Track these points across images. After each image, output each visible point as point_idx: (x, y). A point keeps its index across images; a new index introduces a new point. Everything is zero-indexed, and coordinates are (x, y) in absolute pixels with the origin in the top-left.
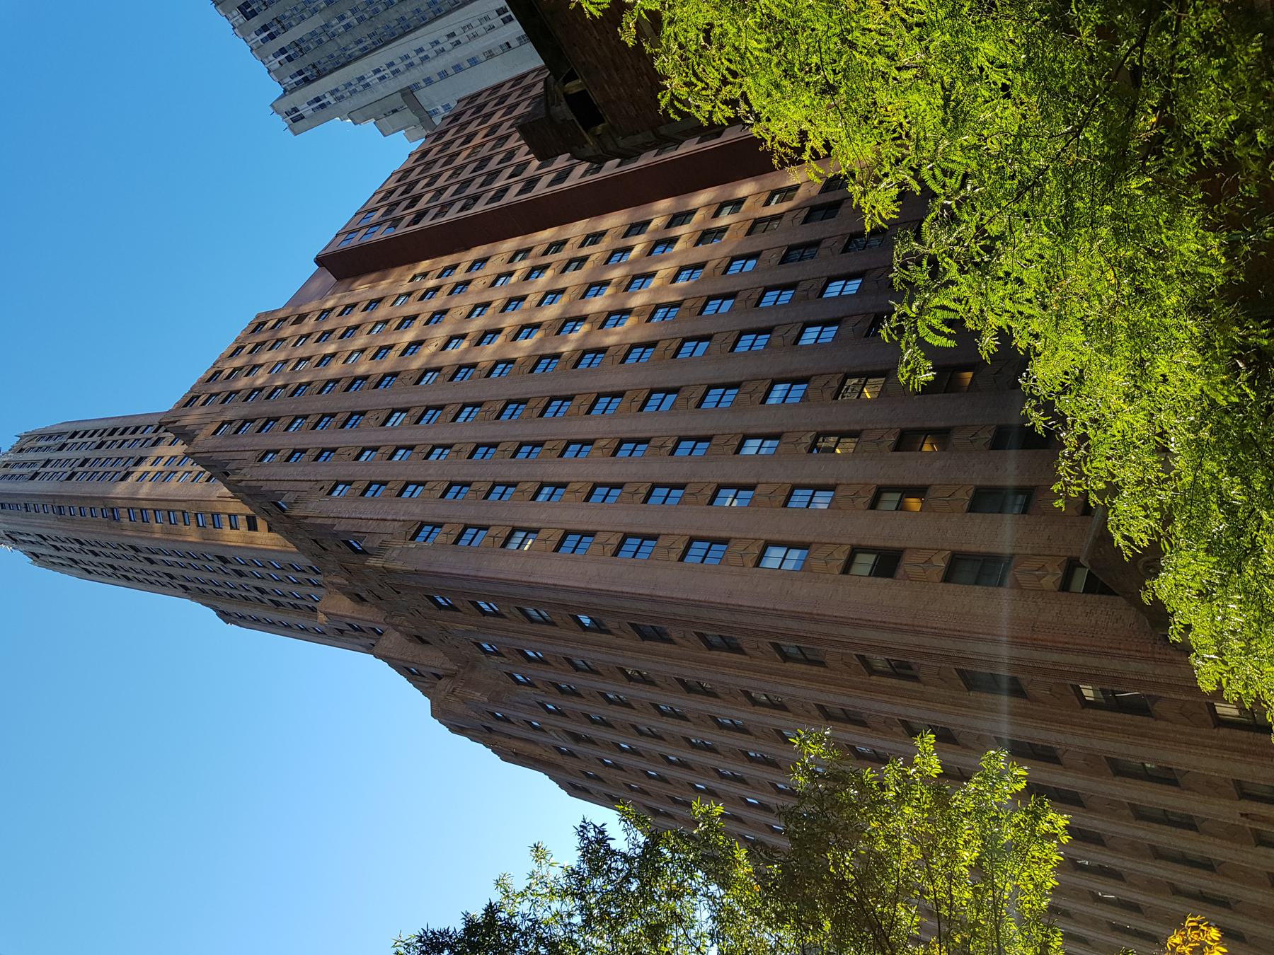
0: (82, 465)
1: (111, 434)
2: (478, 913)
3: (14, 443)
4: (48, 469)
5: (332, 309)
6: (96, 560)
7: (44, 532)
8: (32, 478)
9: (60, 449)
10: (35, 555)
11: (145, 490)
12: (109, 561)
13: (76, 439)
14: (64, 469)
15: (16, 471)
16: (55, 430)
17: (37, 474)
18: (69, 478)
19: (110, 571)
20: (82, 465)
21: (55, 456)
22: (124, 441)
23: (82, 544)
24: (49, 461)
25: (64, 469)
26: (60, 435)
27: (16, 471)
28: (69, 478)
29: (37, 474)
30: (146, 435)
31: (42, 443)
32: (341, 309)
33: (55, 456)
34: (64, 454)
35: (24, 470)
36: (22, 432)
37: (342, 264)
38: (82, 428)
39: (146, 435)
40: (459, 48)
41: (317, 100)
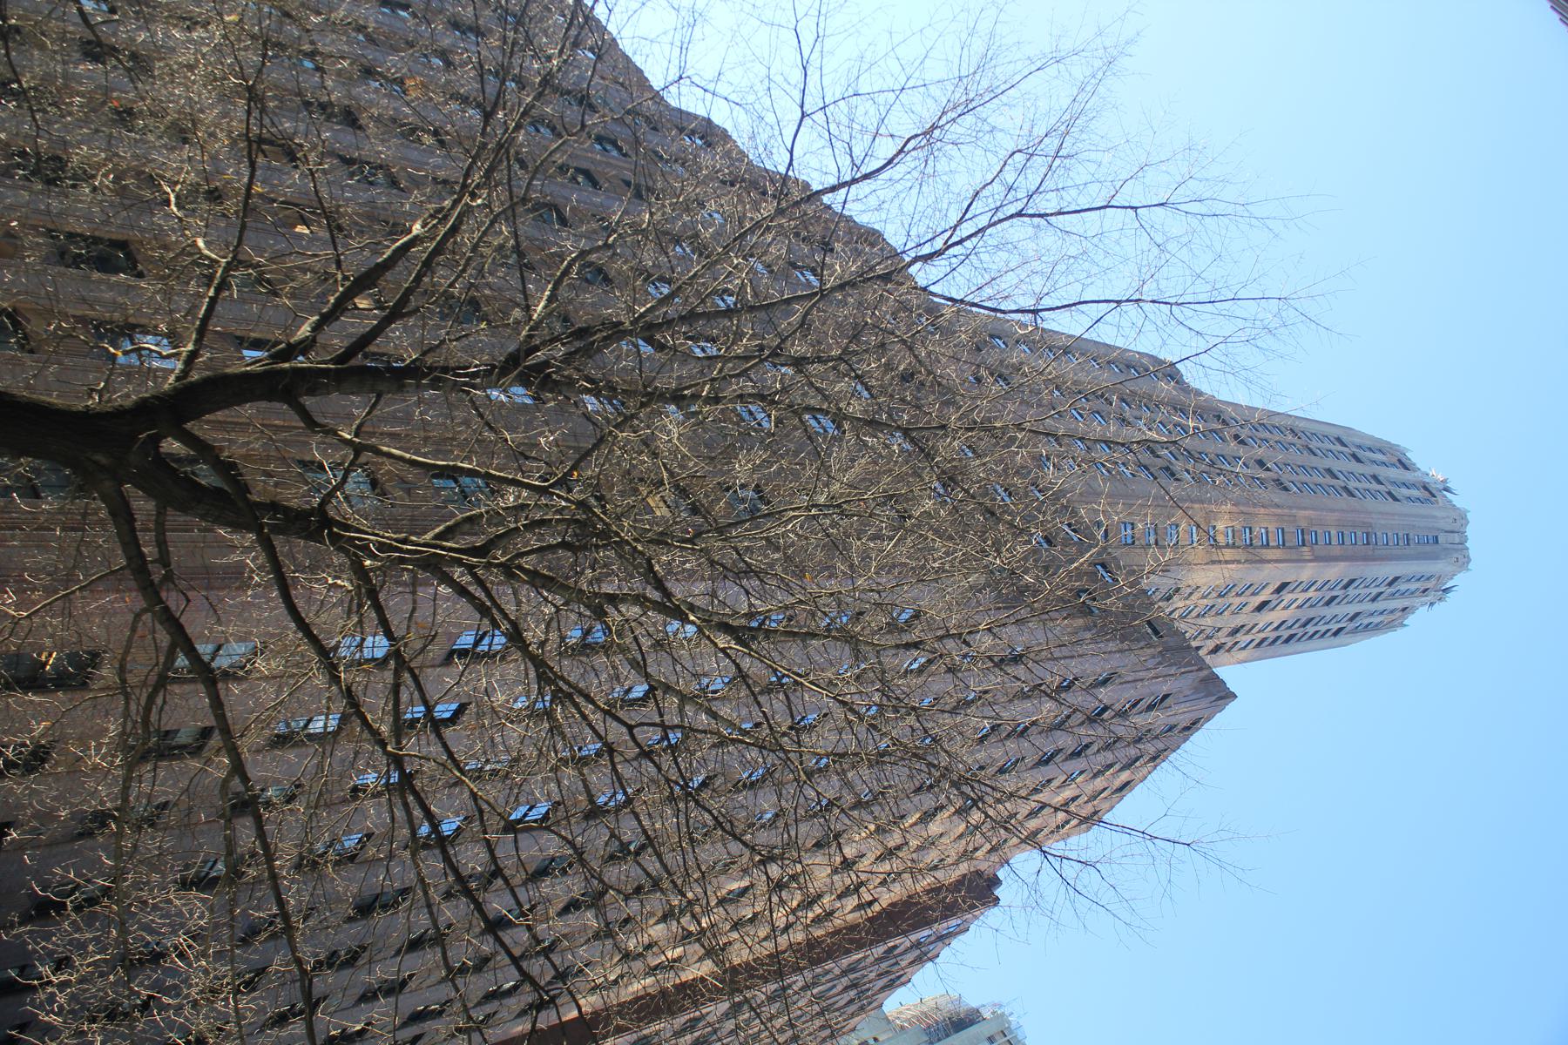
0: (1334, 598)
1: (1292, 636)
2: (998, 892)
3: (1411, 617)
4: (1375, 591)
5: (1122, 769)
6: (1329, 463)
7: (1391, 506)
8: (1396, 579)
9: (1357, 615)
10: (1404, 465)
11: (1307, 572)
12: (1314, 461)
13: (1335, 627)
14: (1357, 592)
15: (1413, 586)
16: (1359, 636)
17: (1390, 584)
18: (1352, 581)
19: (1314, 444)
20: (1334, 598)
21: (1368, 607)
22: (1277, 628)
23: (1346, 489)
24: (1373, 600)
25: (1357, 592)
26: (1355, 631)
27: (1413, 586)
28: (1352, 581)
29: (1390, 584)
30: (1249, 638)
31: (1376, 620)
32: (1089, 752)
33: (1368, 607)
34: (1352, 609)
35: (1403, 587)
36: (1400, 631)
38: (1329, 640)
39: (1249, 638)
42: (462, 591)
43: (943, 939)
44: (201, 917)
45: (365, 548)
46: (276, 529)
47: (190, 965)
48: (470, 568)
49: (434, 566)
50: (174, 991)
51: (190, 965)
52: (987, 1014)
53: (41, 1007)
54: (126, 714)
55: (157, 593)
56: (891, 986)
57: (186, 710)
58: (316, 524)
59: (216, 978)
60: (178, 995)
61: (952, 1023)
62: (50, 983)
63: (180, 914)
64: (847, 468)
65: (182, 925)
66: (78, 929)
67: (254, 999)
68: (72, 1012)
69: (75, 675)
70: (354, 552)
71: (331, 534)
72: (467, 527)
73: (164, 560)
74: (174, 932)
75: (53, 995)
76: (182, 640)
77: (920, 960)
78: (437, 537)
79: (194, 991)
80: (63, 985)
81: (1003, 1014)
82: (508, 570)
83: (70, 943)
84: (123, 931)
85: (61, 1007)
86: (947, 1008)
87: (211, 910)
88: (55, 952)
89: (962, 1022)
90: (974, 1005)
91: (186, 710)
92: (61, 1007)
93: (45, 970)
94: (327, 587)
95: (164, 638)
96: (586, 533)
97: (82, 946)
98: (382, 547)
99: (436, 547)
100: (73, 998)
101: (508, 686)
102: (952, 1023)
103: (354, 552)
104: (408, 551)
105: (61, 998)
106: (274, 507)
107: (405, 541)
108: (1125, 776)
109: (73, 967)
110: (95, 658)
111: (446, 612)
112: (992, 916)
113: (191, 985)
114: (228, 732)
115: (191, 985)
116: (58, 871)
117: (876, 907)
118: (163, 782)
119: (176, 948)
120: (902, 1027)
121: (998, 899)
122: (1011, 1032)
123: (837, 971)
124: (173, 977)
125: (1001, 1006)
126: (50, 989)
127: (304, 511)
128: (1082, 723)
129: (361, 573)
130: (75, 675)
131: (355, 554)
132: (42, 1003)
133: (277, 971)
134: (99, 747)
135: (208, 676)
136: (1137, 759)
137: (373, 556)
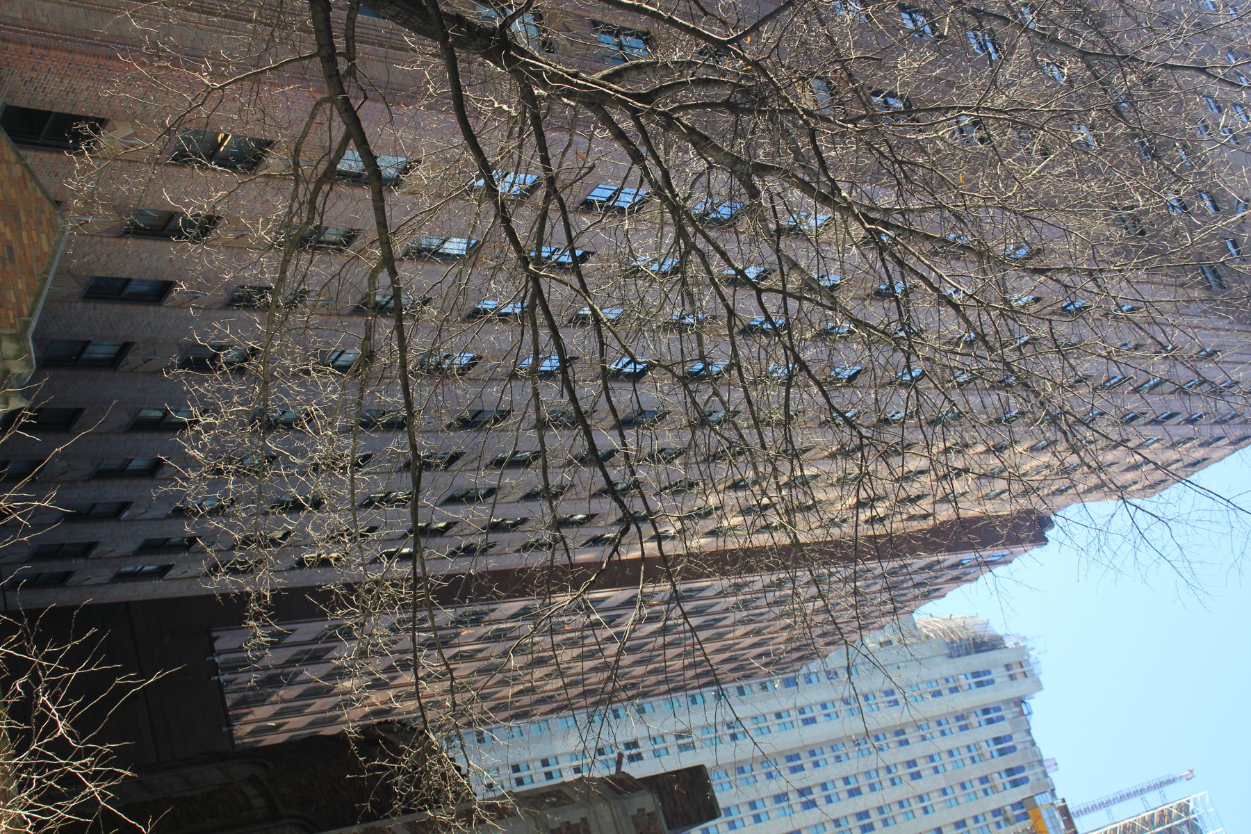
2: (1049, 534)
37: (1031, 529)
40: (778, 708)
41: (980, 684)
42: (620, 135)
43: (989, 564)
44: (334, 391)
45: (538, 75)
46: (463, 44)
47: (317, 433)
48: (635, 112)
49: (596, 102)
50: (301, 453)
51: (317, 433)
52: (1009, 643)
53: (188, 440)
54: (295, 196)
55: (341, 84)
56: (927, 596)
57: (348, 209)
58: (498, 44)
59: (339, 448)
60: (302, 457)
61: (975, 643)
62: (197, 422)
63: (315, 384)
64: (1018, 81)
65: (316, 395)
66: (227, 380)
67: (369, 473)
68: (212, 450)
69: (247, 158)
70: (525, 76)
71: (507, 56)
72: (634, 73)
73: (350, 55)
74: (308, 402)
75: (199, 433)
76: (356, 134)
77: (957, 580)
78: (605, 78)
79: (316, 456)
80: (209, 427)
81: (1024, 647)
82: (669, 121)
83: (219, 390)
84: (265, 389)
85: (204, 445)
86: (975, 629)
87: (344, 388)
88: (204, 396)
89: (983, 644)
90: (1000, 631)
91: (348, 209)
92: (204, 445)
93: (195, 411)
94: (496, 102)
95: (339, 128)
96: (751, 98)
97: (228, 396)
98: (554, 76)
99: (604, 86)
100: (215, 439)
101: (650, 245)
102: (975, 643)
103: (525, 76)
104: (577, 85)
105: (205, 437)
106: (459, 20)
107: (576, 76)
108: (1199, 454)
109: (218, 412)
110: (265, 145)
111: (606, 168)
112: (1036, 551)
113: (315, 451)
114: (385, 226)
115: (315, 451)
116: (216, 325)
117: (931, 521)
118: (317, 269)
119: (308, 415)
120: (927, 637)
121: (1046, 540)
122: (1029, 665)
123: (878, 571)
124: (301, 440)
125: (1024, 639)
126: (197, 428)
127: (486, 29)
128: (1173, 393)
129: (528, 97)
130: (247, 158)
131: (527, 78)
132: (189, 438)
133: (393, 452)
134: (267, 221)
135: (373, 178)
136: (1219, 439)
137: (544, 85)
